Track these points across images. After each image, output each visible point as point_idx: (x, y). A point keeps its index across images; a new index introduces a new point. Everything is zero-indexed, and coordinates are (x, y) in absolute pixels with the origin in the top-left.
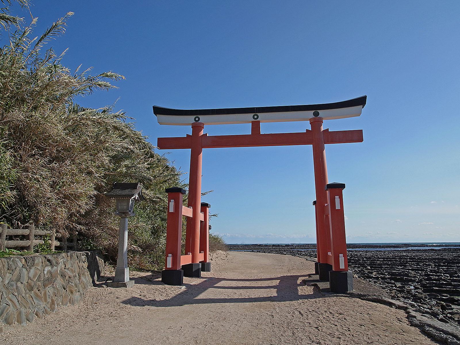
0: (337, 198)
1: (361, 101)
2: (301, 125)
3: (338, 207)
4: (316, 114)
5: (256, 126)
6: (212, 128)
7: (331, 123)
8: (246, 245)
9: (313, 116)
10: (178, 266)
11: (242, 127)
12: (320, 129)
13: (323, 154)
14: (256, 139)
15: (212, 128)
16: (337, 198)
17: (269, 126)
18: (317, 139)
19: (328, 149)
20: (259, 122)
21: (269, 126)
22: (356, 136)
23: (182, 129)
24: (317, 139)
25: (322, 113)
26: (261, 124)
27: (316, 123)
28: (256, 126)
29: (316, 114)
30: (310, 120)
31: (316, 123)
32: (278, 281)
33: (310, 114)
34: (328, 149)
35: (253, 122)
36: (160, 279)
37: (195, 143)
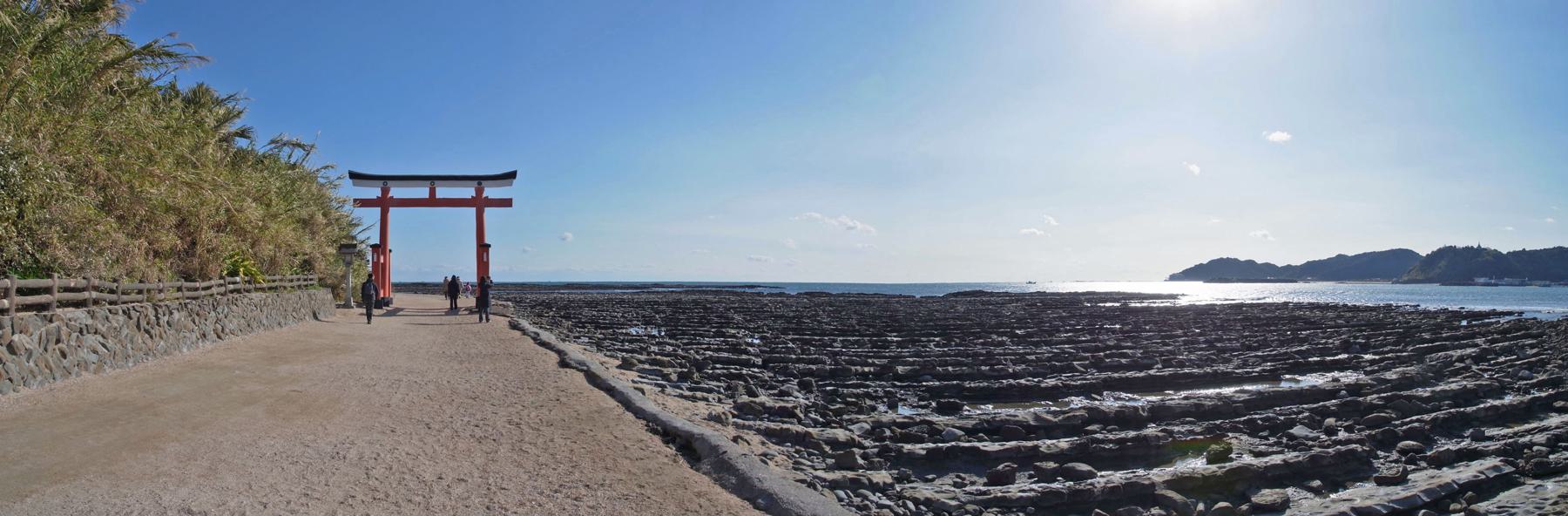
2: (468, 192)
5: (432, 192)
6: (397, 192)
7: (491, 192)
8: (424, 285)
10: (1398, 287)
11: (422, 192)
12: (483, 194)
14: (432, 202)
15: (397, 192)
17: (443, 192)
18: (480, 203)
21: (443, 192)
22: (507, 203)
23: (374, 192)
24: (480, 203)
28: (432, 192)
31: (479, 191)
32: (1452, 507)
34: (488, 211)
37: (384, 203)
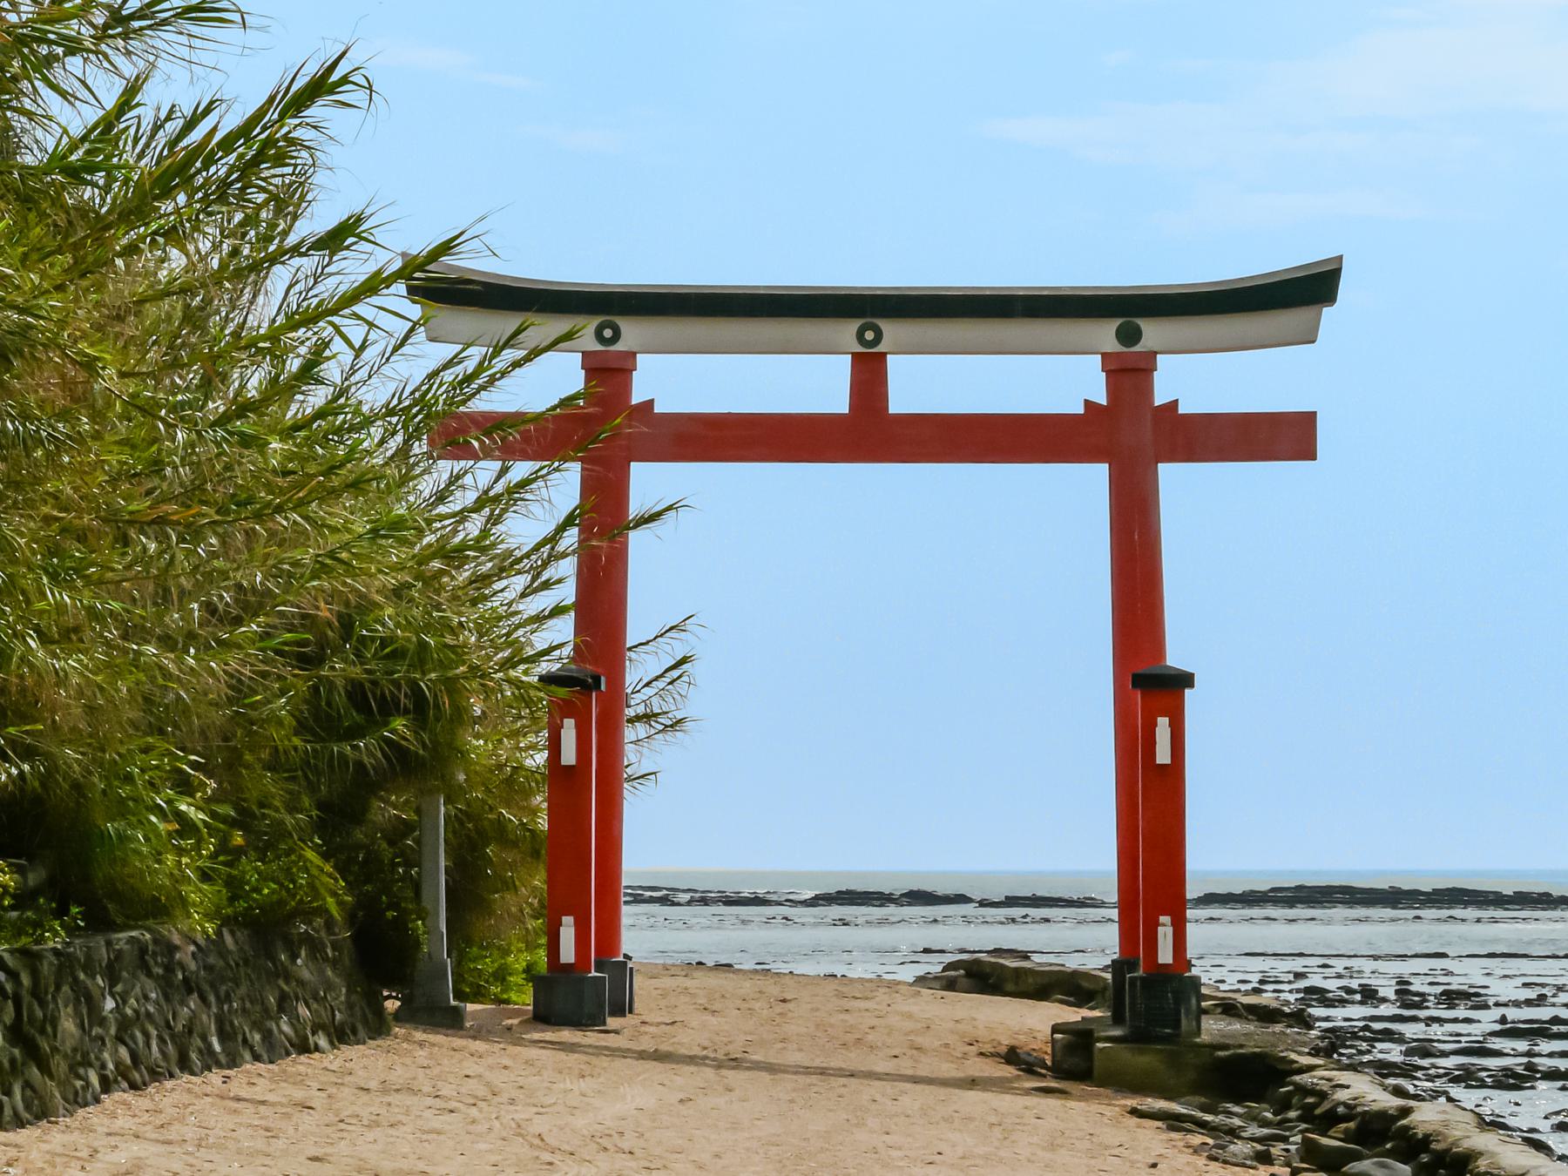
0: (1163, 723)
1: (1314, 287)
2: (1067, 380)
3: (1163, 756)
4: (1129, 336)
5: (869, 375)
6: (671, 379)
7: (1191, 379)
9: (1112, 345)
11: (815, 381)
13: (1273, 308)
14: (869, 431)
15: (671, 379)
16: (1163, 723)
17: (923, 381)
18: (1130, 439)
19: (1180, 486)
20: (882, 356)
21: (923, 381)
22: (1285, 436)
24: (1130, 439)
25: (1153, 332)
26: (891, 359)
27: (1129, 374)
28: (869, 375)
29: (1129, 336)
30: (1105, 356)
33: (1105, 333)
35: (856, 357)
36: (1099, 1045)
